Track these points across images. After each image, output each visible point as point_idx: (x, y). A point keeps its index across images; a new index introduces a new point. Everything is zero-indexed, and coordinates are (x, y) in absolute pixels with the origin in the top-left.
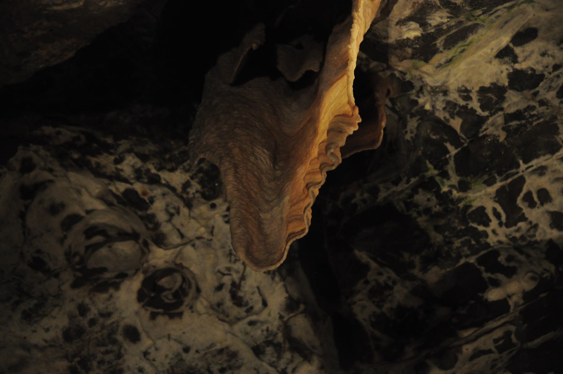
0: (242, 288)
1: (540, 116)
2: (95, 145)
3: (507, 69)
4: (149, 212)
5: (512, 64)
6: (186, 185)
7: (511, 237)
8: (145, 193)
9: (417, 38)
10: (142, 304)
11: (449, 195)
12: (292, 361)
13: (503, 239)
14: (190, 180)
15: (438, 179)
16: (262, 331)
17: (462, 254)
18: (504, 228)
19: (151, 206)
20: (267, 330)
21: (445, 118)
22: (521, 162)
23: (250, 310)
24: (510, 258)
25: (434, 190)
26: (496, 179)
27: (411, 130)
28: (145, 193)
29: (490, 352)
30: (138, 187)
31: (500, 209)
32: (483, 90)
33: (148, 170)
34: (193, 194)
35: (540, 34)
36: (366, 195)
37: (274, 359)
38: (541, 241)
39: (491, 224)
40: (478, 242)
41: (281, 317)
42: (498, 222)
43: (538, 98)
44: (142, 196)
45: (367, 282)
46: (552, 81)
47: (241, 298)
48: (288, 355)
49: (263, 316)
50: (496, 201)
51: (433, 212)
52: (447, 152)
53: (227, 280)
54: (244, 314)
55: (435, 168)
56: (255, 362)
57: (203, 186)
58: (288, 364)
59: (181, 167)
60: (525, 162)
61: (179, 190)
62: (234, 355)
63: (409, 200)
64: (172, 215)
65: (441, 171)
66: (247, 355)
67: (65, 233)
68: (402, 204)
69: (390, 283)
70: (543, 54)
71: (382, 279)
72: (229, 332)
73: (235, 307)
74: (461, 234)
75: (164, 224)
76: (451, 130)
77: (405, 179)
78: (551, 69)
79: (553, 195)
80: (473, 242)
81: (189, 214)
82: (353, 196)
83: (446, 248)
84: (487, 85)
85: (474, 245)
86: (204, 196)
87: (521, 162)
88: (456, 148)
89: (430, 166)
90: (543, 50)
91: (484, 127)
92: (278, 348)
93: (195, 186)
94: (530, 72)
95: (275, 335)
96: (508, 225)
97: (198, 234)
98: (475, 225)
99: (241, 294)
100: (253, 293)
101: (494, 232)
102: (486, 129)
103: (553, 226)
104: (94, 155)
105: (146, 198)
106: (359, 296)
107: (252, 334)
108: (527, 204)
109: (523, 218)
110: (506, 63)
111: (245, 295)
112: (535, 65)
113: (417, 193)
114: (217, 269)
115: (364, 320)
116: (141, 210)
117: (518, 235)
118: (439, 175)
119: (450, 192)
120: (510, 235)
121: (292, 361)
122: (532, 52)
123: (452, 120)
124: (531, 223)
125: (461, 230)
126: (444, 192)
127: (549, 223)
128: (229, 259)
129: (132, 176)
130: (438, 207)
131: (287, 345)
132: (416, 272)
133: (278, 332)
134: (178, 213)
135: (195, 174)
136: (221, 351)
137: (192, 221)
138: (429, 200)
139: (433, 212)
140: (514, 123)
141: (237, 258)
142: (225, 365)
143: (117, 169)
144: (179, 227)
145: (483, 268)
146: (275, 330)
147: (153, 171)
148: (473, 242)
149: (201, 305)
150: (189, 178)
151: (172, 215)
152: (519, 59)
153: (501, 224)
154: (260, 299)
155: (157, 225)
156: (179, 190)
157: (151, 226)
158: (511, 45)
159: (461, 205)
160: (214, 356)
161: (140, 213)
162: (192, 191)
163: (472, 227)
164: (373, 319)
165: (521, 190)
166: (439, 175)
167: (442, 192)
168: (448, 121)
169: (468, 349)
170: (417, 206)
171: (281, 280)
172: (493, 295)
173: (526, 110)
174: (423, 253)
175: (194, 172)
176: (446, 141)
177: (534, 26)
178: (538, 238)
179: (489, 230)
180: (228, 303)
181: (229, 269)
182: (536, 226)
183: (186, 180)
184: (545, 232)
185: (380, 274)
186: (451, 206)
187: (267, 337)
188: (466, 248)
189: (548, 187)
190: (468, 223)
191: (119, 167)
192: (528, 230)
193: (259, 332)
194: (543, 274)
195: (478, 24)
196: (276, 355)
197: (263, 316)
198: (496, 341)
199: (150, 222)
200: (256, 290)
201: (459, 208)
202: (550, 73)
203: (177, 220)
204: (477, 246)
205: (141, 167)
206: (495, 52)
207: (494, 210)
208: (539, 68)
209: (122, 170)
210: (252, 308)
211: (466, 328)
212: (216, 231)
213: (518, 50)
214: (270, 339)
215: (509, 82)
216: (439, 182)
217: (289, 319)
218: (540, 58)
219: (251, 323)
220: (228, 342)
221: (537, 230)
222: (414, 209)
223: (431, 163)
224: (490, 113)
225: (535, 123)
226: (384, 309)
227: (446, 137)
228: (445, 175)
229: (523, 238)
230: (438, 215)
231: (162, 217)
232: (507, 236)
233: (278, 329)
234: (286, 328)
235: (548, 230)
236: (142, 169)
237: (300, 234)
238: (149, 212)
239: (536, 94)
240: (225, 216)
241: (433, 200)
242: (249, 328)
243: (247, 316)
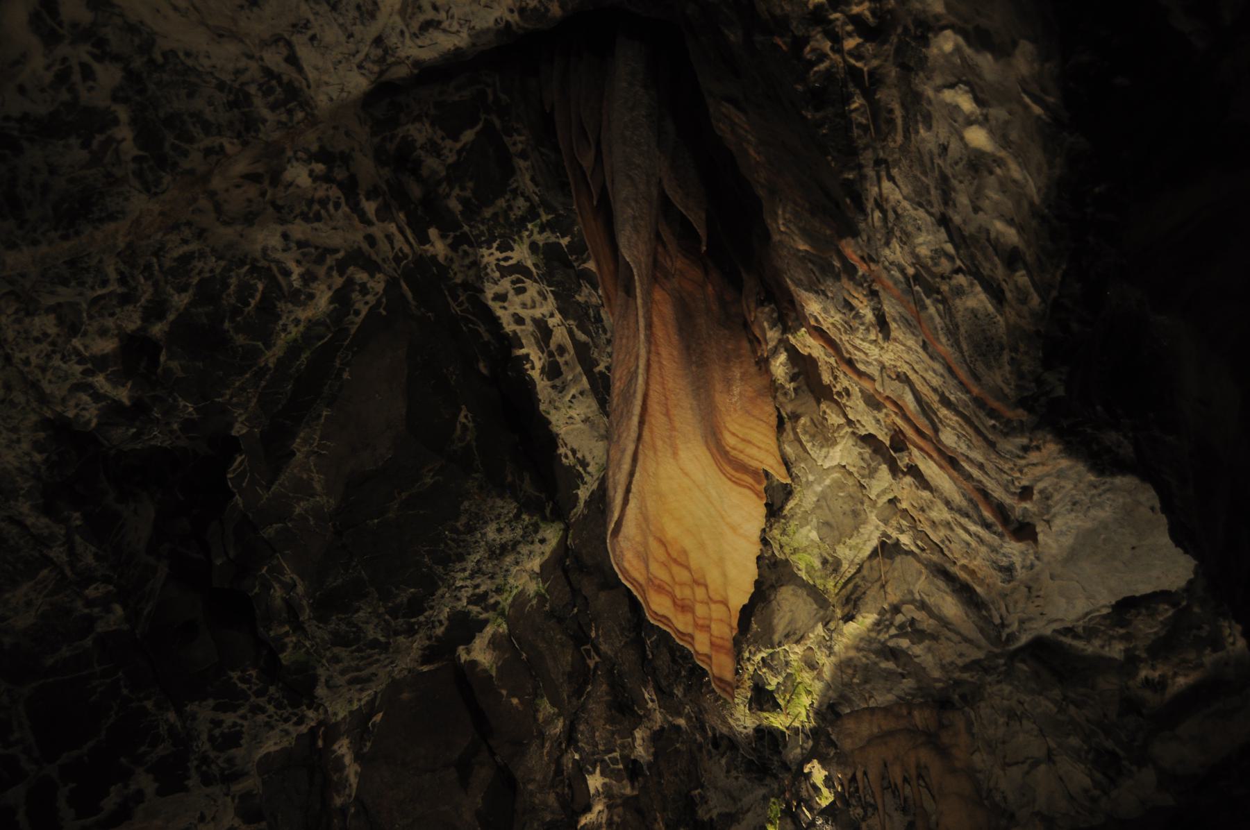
12: (371, 73)
13: (485, 260)
15: (538, 221)
18: (495, 262)
20: (397, 48)
23: (415, 36)
29: (393, 248)
31: (511, 262)
36: (520, 146)
37: (372, 57)
38: (484, 286)
39: (498, 252)
41: (408, 58)
45: (443, 139)
47: (427, 30)
48: (376, 69)
49: (408, 42)
50: (518, 262)
52: (563, 236)
53: (443, 15)
54: (412, 31)
55: (548, 221)
56: (369, 40)
57: (532, 10)
58: (369, 70)
62: (373, 16)
63: (519, 192)
66: (373, 30)
68: (514, 185)
69: (443, 158)
71: (446, 151)
72: (392, 10)
73: (419, 24)
77: (537, 190)
80: (483, 239)
82: (520, 134)
89: (550, 217)
91: (589, 286)
95: (393, 56)
98: (498, 242)
99: (431, 30)
100: (431, 39)
101: (492, 254)
102: (586, 287)
106: (430, 131)
109: (502, 276)
113: (526, 201)
114: (452, 6)
115: (408, 130)
117: (489, 270)
118: (542, 223)
119: (527, 230)
121: (371, 73)
124: (499, 280)
128: (462, 18)
130: (514, 217)
132: (456, 191)
138: (519, 208)
142: (364, 9)
146: (397, 55)
153: (498, 260)
154: (425, 44)
159: (516, 238)
164: (410, 139)
166: (542, 223)
169: (392, 228)
170: (514, 199)
172: (433, 233)
173: (603, 327)
174: (474, 200)
178: (486, 284)
179: (493, 250)
180: (422, 18)
181: (452, 17)
182: (496, 283)
184: (492, 289)
185: (451, 150)
186: (515, 229)
190: (500, 238)
192: (493, 278)
194: (452, 270)
196: (376, 58)
197: (408, 42)
198: (401, 249)
207: (511, 258)
210: (418, 37)
211: (407, 216)
212: (489, 10)
214: (390, 52)
216: (536, 222)
219: (402, 33)
226: (419, 152)
227: (576, 239)
228: (542, 229)
229: (487, 274)
230: (507, 218)
232: (488, 263)
233: (398, 57)
234: (399, 62)
235: (493, 291)
240: (501, 19)
242: (398, 30)
243: (410, 33)
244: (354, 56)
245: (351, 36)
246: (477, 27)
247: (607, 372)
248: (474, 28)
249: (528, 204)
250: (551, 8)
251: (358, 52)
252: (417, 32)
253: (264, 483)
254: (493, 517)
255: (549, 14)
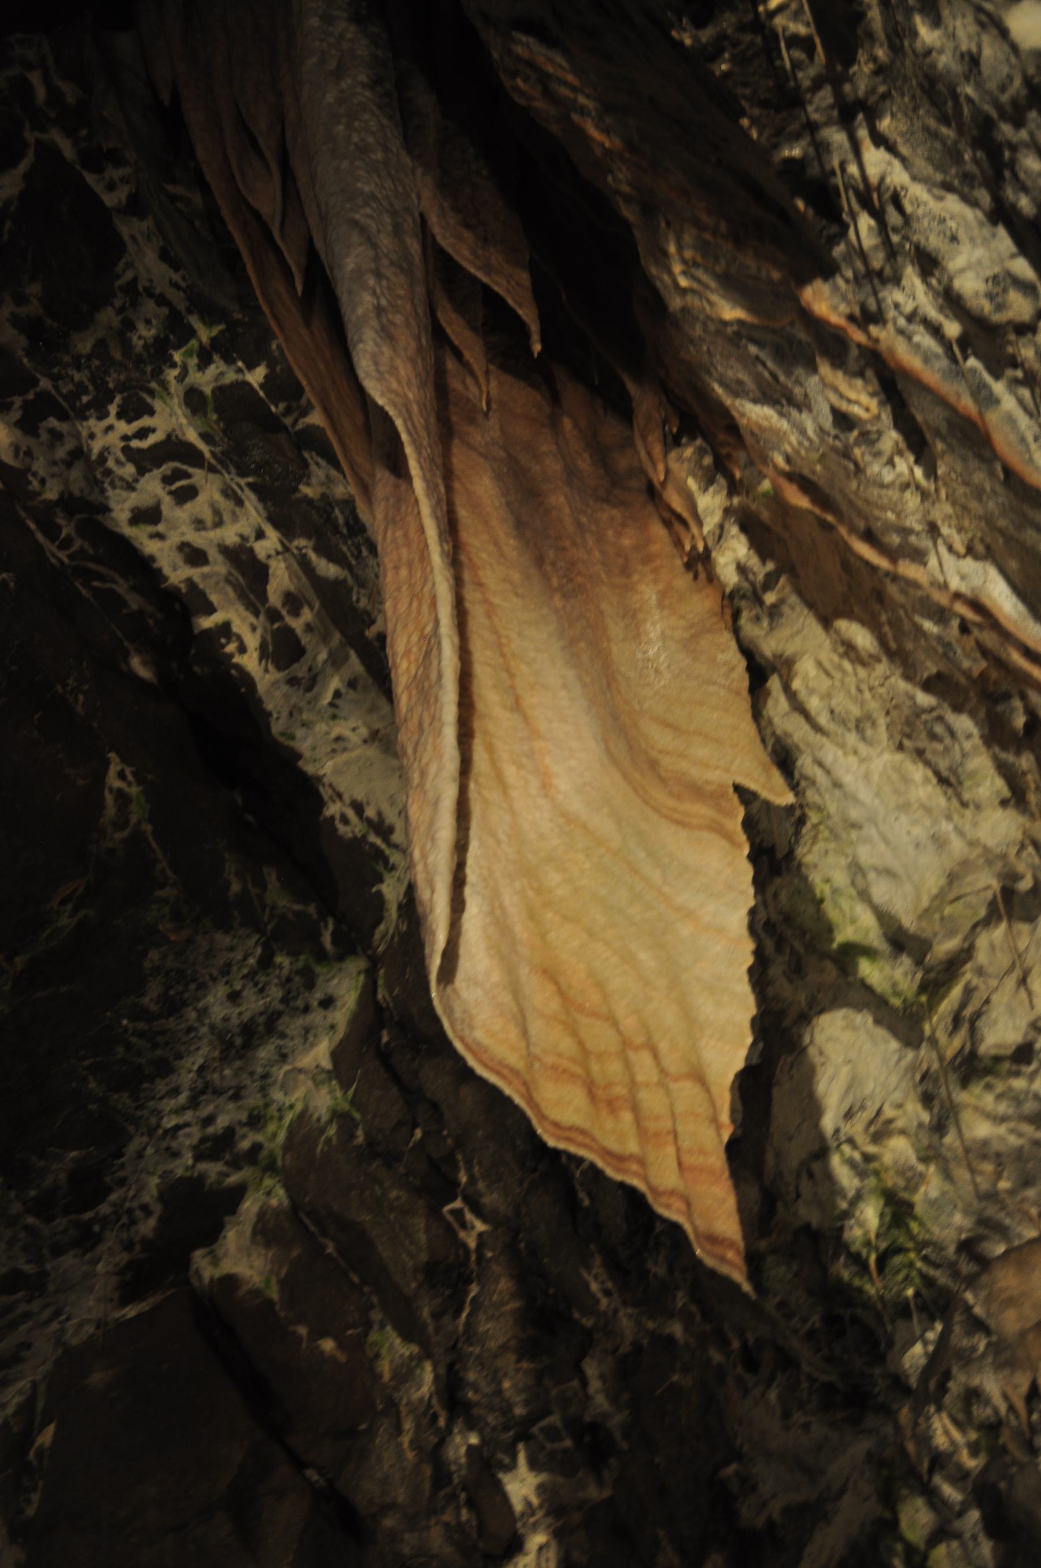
1: (658, 1268)
7: (106, 454)
11: (168, 364)
15: (193, 343)
17: (60, 382)
24: (56, 436)
25: (172, 337)
31: (152, 439)
38: (107, 498)
40: (88, 406)
42: (130, 434)
50: (169, 436)
51: (129, 334)
55: (213, 340)
65: (208, 348)
68: (129, 275)
74: (99, 382)
79: (188, 506)
80: (85, 399)
83: (66, 358)
85: (80, 400)
88: (262, 386)
89: (215, 331)
96: (126, 450)
101: (110, 428)
102: (317, 464)
103: (136, 511)
108: (169, 473)
117: (111, 464)
118: (201, 346)
119: (174, 365)
120: (109, 453)
125: (107, 383)
126: (171, 357)
127: (140, 505)
130: (141, 343)
139: (129, 334)
145: (31, 396)
148: (85, 399)
153: (125, 438)
159: (153, 385)
163: (114, 397)
165: (191, 465)
166: (201, 346)
167: (172, 352)
170: (134, 304)
176: (271, 366)
178: (110, 493)
179: (111, 420)
186: (149, 369)
188: (71, 387)
189: (202, 498)
190: (121, 392)
192: (122, 479)
194: (34, 475)
204: (78, 404)
221: (125, 489)
222: (127, 299)
223: (221, 332)
229: (108, 472)
230: (126, 345)
235: (129, 505)
241: (150, 330)
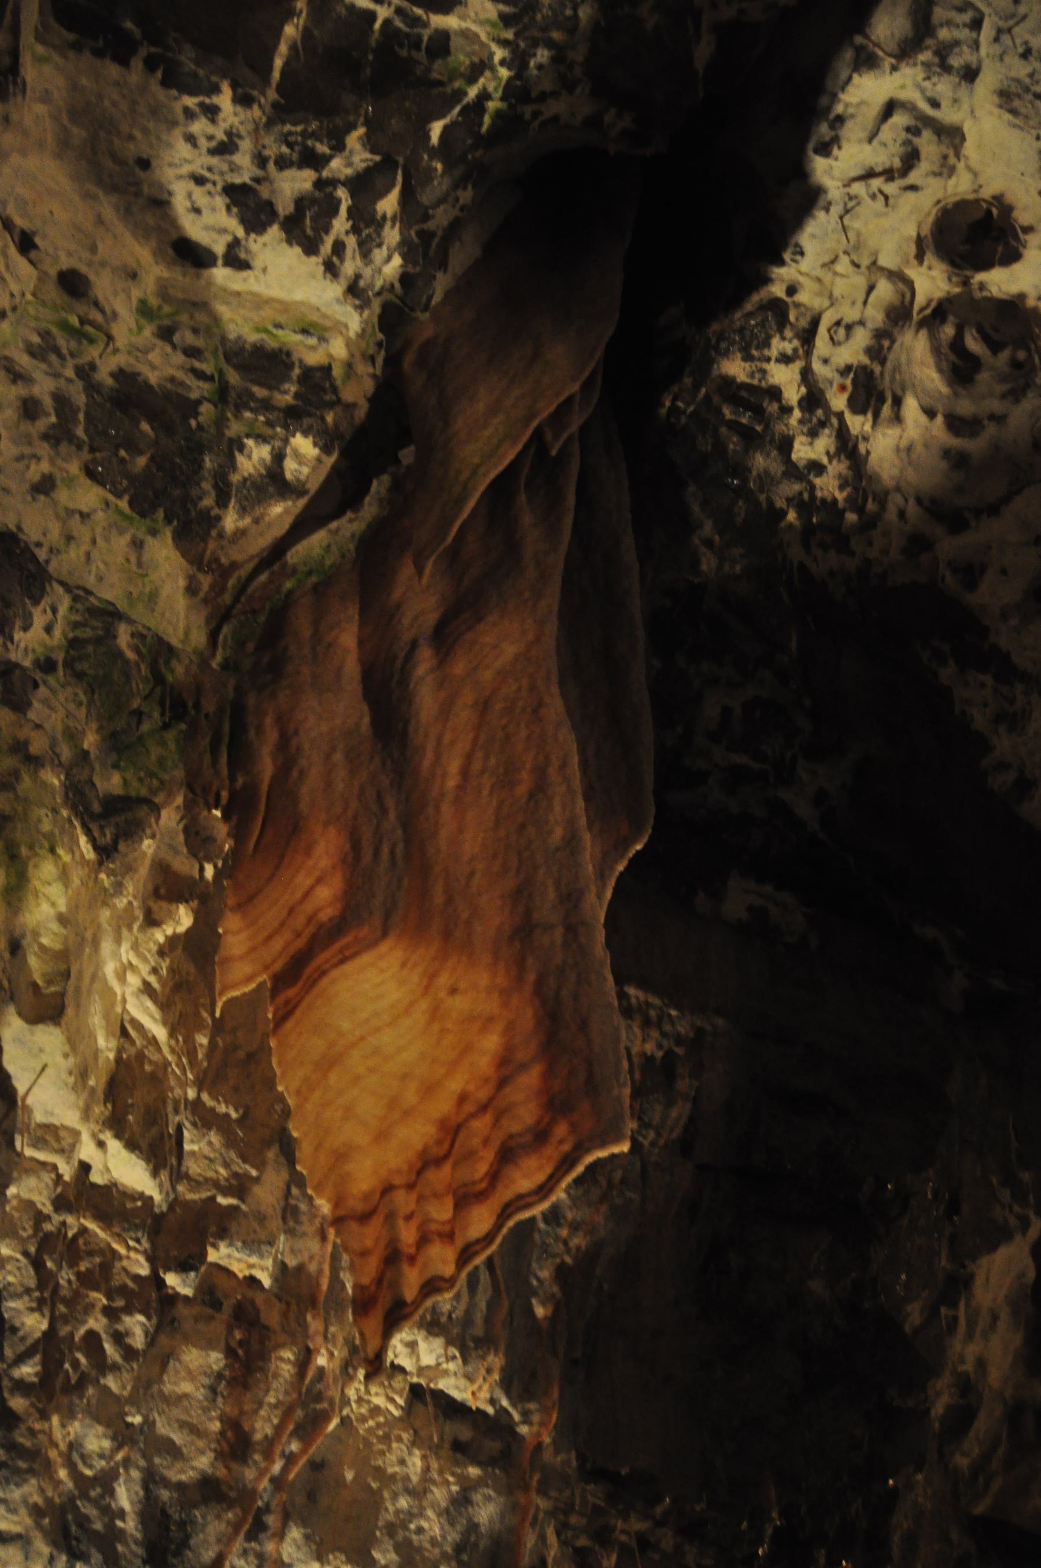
0: (887, 165)
2: (814, 520)
3: (255, 241)
4: (865, 360)
5: (243, 242)
6: (785, 359)
8: (843, 388)
9: (305, 434)
10: (1021, 249)
12: (949, 23)
14: (773, 359)
16: (934, 84)
19: (855, 363)
21: (393, 227)
22: (377, 25)
26: (430, 38)
27: (454, 206)
28: (843, 388)
30: (839, 402)
32: (310, 248)
33: (801, 422)
34: (790, 341)
35: (174, 236)
37: (965, 48)
41: (894, 68)
43: (259, 173)
44: (850, 387)
46: (222, 173)
48: (944, 34)
49: (910, 94)
58: (958, 26)
59: (763, 384)
60: (372, 16)
61: (798, 365)
64: (849, 328)
67: (986, 422)
70: (197, 211)
75: (870, 325)
76: (407, 197)
78: (209, 186)
81: (827, 309)
84: (297, 250)
86: (782, 321)
87: (377, 25)
90: (192, 216)
92: (943, 53)
93: (778, 345)
94: (235, 210)
97: (851, 269)
99: (897, 163)
104: (835, 501)
105: (848, 382)
107: (950, 94)
110: (248, 251)
111: (893, 156)
112: (220, 210)
114: (885, 210)
116: (872, 372)
119: (503, 63)
122: (207, 228)
123: (389, 215)
126: (509, 69)
128: (857, 209)
129: (827, 431)
131: (929, 42)
133: (919, 62)
134: (838, 323)
135: (759, 359)
136: (1014, 112)
137: (837, 293)
140: (322, 148)
141: (847, 199)
143: (830, 462)
144: (859, 304)
147: (797, 414)
149: (960, 186)
150: (772, 363)
151: (849, 328)
152: (229, 238)
154: (886, 128)
155: (880, 334)
156: (798, 365)
157: (886, 343)
158: (220, 262)
159: (509, 35)
160: (1027, 117)
161: (877, 369)
162: (788, 347)
168: (394, 219)
171: (839, 101)
175: (759, 364)
177: (170, 252)
180: (924, 166)
181: (873, 197)
183: (778, 365)
187: (939, 75)
191: (825, 460)
193: (940, 87)
195: (227, 358)
196: (956, 50)
199: (882, 347)
200: (875, 142)
201: (516, 34)
202: (214, 183)
203: (851, 315)
205: (803, 434)
206: (245, 274)
208: (220, 201)
209: (828, 453)
210: (908, 129)
212: (827, 259)
213: (219, 249)
214: (938, 70)
215: (270, 225)
217: (890, 55)
218: (205, 212)
219: (935, 104)
220: (989, 107)
224: (335, 188)
225: (299, 128)
231: (862, 338)
234: (905, 51)
236: (805, 430)
237: (528, 1206)
238: (865, 360)
239: (257, 180)
242: (944, 104)
244: (999, 31)
245: (1026, 55)
246: (821, 215)
247: (207, 101)
248: (827, 210)
249: (534, 95)
250: (743, 364)
251: (996, 40)
252: (916, 141)
253: (1000, 249)
254: (350, 266)
255: (739, 355)
